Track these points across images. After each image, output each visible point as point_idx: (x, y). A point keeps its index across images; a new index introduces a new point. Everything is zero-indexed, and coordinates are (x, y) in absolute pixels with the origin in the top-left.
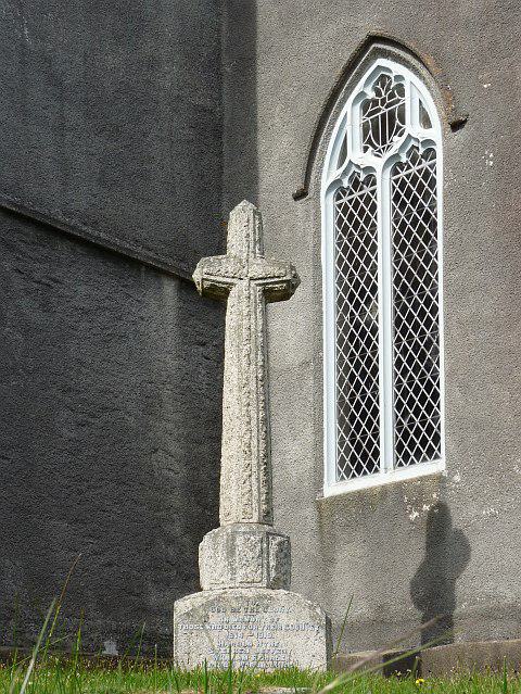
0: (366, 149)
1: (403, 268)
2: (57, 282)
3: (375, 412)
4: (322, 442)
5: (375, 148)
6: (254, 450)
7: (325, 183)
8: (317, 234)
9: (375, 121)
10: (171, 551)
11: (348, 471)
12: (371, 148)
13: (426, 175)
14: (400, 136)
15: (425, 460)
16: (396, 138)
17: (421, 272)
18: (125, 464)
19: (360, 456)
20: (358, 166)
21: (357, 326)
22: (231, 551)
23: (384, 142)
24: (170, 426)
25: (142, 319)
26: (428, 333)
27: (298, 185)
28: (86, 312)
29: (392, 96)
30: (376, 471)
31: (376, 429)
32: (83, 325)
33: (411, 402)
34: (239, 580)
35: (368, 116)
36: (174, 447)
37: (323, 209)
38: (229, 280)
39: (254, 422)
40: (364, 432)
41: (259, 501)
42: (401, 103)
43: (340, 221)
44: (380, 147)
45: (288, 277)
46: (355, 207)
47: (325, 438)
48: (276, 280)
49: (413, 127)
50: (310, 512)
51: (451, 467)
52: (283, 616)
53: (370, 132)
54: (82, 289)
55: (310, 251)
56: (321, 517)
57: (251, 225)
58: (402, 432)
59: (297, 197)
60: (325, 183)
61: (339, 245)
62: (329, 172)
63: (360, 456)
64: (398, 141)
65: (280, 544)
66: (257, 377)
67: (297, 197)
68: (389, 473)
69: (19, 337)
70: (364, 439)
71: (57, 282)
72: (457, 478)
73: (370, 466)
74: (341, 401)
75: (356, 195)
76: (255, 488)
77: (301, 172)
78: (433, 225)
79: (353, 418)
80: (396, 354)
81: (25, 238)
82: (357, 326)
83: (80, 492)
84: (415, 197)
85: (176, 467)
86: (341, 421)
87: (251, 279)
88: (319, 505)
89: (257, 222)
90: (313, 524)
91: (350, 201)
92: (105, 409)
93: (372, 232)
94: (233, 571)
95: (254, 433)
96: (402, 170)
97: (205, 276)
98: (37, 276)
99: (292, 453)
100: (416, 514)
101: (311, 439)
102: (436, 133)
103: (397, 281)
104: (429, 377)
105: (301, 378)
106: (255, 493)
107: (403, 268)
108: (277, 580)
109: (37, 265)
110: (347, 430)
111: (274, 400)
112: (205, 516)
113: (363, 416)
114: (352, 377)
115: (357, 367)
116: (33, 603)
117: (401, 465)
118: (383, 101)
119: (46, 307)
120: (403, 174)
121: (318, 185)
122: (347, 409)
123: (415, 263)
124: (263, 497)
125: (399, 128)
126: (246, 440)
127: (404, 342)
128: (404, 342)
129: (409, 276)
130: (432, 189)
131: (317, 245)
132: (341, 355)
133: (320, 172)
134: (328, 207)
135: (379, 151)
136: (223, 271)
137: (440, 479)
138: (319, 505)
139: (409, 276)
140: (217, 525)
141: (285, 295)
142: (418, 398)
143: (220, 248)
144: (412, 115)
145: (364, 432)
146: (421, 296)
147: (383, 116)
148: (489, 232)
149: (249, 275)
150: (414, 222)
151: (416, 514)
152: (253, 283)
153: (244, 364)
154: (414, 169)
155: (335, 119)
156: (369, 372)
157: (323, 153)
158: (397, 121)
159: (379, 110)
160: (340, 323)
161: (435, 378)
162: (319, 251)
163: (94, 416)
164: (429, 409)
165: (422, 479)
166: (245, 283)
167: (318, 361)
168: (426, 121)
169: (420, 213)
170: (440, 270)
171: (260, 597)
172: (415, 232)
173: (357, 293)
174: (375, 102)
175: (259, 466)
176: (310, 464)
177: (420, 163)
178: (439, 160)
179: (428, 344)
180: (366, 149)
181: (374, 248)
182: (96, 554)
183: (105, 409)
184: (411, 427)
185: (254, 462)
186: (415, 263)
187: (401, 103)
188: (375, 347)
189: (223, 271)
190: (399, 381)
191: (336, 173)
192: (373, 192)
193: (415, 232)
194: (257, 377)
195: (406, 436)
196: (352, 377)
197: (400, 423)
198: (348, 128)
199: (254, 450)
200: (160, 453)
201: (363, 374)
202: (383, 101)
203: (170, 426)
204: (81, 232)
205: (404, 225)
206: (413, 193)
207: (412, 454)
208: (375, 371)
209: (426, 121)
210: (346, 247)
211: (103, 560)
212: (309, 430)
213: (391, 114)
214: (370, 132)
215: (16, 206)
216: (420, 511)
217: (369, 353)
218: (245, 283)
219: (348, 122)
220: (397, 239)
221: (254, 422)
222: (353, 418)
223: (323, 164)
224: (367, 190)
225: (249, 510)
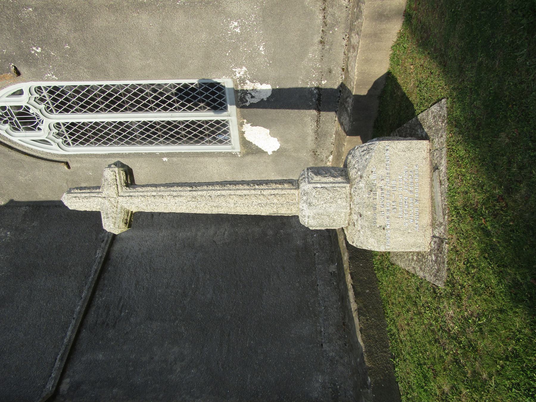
1: (108, 106)
3: (193, 122)
5: (38, 124)
9: (23, 124)
10: (270, 232)
12: (39, 126)
14: (29, 108)
16: (31, 111)
17: (110, 95)
20: (49, 133)
23: (34, 118)
24: (199, 234)
25: (140, 249)
26: (147, 91)
29: (6, 114)
31: (203, 122)
35: (20, 128)
36: (211, 232)
40: (204, 129)
41: (282, 189)
42: (10, 108)
43: (82, 143)
46: (73, 135)
47: (207, 151)
48: (118, 177)
49: (22, 101)
53: (29, 126)
55: (100, 160)
57: (79, 195)
59: (69, 167)
60: (62, 152)
62: (55, 149)
66: (190, 191)
67: (69, 167)
70: (208, 129)
73: (224, 125)
74: (186, 143)
75: (66, 134)
76: (273, 192)
78: (82, 88)
79: (196, 136)
80: (159, 111)
84: (82, 134)
85: (222, 230)
89: (76, 191)
93: (88, 125)
95: (232, 192)
96: (50, 107)
97: (117, 226)
99: (217, 170)
102: (25, 86)
103: (116, 110)
106: (276, 192)
107: (108, 106)
110: (202, 139)
111: (188, 181)
112: (285, 224)
113: (195, 130)
114: (172, 136)
115: (166, 133)
116: (315, 315)
118: (10, 119)
121: (62, 156)
122: (190, 139)
123: (105, 99)
125: (25, 110)
127: (152, 105)
128: (152, 105)
129: (113, 102)
130: (60, 89)
131: (96, 156)
132: (159, 142)
133: (54, 155)
135: (40, 121)
139: (113, 102)
140: (298, 217)
141: (129, 172)
143: (95, 217)
145: (204, 129)
146: (125, 95)
147: (19, 119)
149: (115, 196)
150: (80, 100)
154: (48, 100)
155: (22, 146)
156: (169, 127)
158: (21, 111)
160: (141, 143)
161: (175, 87)
168: (20, 93)
169: (75, 97)
170: (109, 83)
172: (87, 99)
173: (123, 133)
177: (44, 96)
178: (43, 84)
180: (39, 129)
181: (97, 124)
186: (105, 99)
187: (10, 108)
188: (155, 123)
191: (55, 146)
193: (87, 99)
194: (190, 191)
196: (172, 136)
198: (28, 139)
200: (215, 239)
201: (171, 130)
202: (10, 119)
203: (199, 234)
205: (82, 106)
206: (60, 100)
207: (220, 101)
208: (169, 123)
209: (20, 93)
210: (97, 140)
214: (29, 126)
217: (158, 127)
220: (91, 110)
221: (223, 193)
222: (196, 136)
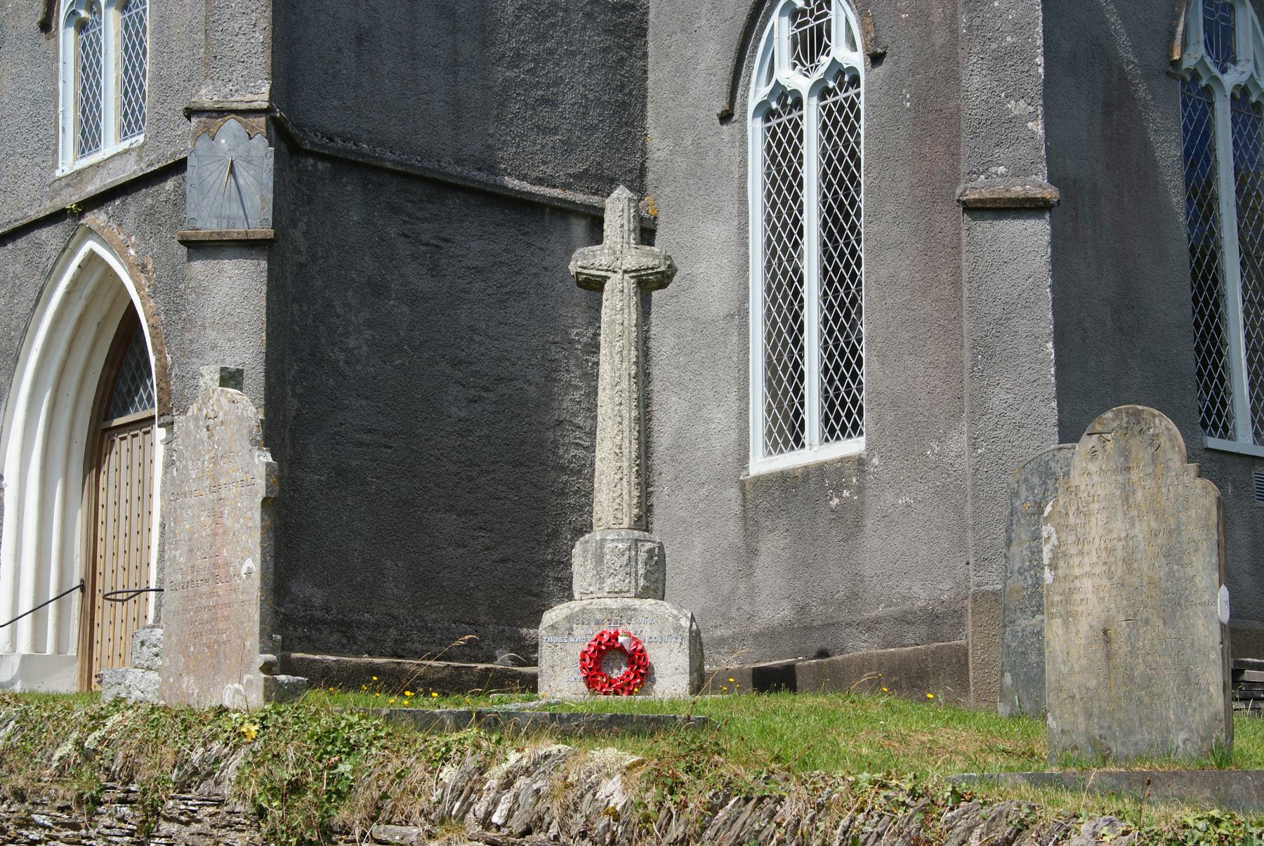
0: (795, 66)
2: (447, 240)
4: (747, 409)
6: (626, 451)
7: (752, 105)
8: (744, 163)
9: (803, 33)
11: (775, 445)
12: (799, 67)
13: (853, 105)
15: (850, 436)
17: (847, 217)
18: (523, 442)
19: (789, 430)
21: (785, 273)
22: (600, 559)
23: (812, 61)
25: (546, 269)
27: (720, 105)
28: (479, 271)
30: (803, 446)
32: (478, 285)
33: (837, 368)
34: (607, 589)
35: (797, 27)
37: (749, 133)
38: (603, 273)
39: (626, 422)
41: (629, 505)
44: (808, 65)
45: (662, 269)
47: (751, 405)
50: (733, 493)
51: (870, 447)
52: (647, 628)
54: (476, 245)
56: (744, 499)
57: (626, 215)
58: (829, 403)
61: (768, 175)
62: (757, 92)
63: (789, 430)
64: (825, 61)
65: (650, 551)
68: (817, 450)
69: (406, 309)
71: (447, 240)
72: (876, 461)
74: (769, 362)
76: (625, 492)
77: (725, 89)
81: (412, 198)
82: (785, 273)
83: (470, 479)
86: (769, 385)
87: (625, 272)
88: (742, 485)
90: (736, 508)
91: (779, 125)
92: (500, 380)
94: (602, 580)
95: (626, 434)
97: (579, 270)
98: (424, 238)
100: (836, 501)
101: (735, 406)
104: (853, 340)
105: (725, 333)
106: (626, 497)
108: (645, 588)
109: (426, 225)
117: (827, 440)
118: (812, 12)
119: (435, 271)
120: (830, 100)
121: (745, 105)
123: (841, 206)
124: (635, 501)
126: (617, 441)
129: (836, 221)
131: (744, 176)
134: (756, 129)
136: (597, 264)
137: (860, 463)
138: (742, 485)
139: (836, 221)
142: (843, 363)
144: (838, 32)
148: (905, 183)
151: (836, 501)
152: (627, 276)
153: (617, 358)
155: (756, 47)
157: (750, 68)
159: (807, 22)
162: (745, 183)
163: (487, 390)
164: (854, 376)
165: (843, 460)
166: (619, 276)
167: (742, 313)
171: (624, 609)
173: (785, 232)
174: (803, 12)
175: (631, 468)
176: (734, 436)
179: (854, 301)
180: (795, 66)
182: (488, 549)
183: (500, 380)
184: (837, 396)
185: (626, 464)
186: (841, 206)
189: (597, 264)
190: (826, 342)
192: (801, 117)
195: (831, 406)
197: (826, 391)
199: (626, 451)
204: (474, 181)
211: (496, 556)
212: (733, 396)
213: (819, 27)
215: (402, 165)
216: (840, 497)
218: (619, 276)
219: (776, 35)
221: (626, 422)
223: (749, 81)
224: (795, 114)
225: (619, 515)
